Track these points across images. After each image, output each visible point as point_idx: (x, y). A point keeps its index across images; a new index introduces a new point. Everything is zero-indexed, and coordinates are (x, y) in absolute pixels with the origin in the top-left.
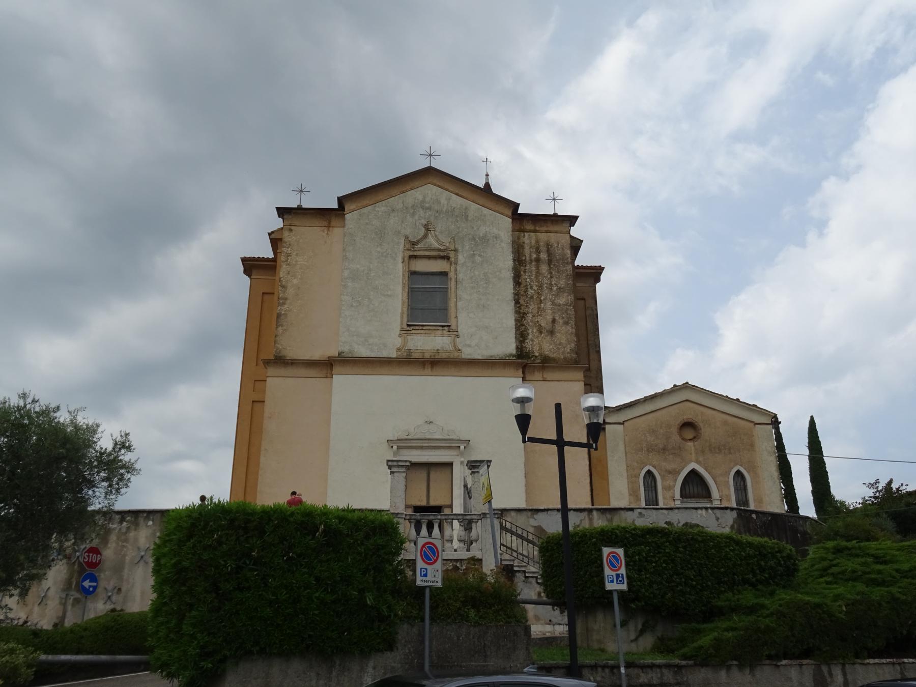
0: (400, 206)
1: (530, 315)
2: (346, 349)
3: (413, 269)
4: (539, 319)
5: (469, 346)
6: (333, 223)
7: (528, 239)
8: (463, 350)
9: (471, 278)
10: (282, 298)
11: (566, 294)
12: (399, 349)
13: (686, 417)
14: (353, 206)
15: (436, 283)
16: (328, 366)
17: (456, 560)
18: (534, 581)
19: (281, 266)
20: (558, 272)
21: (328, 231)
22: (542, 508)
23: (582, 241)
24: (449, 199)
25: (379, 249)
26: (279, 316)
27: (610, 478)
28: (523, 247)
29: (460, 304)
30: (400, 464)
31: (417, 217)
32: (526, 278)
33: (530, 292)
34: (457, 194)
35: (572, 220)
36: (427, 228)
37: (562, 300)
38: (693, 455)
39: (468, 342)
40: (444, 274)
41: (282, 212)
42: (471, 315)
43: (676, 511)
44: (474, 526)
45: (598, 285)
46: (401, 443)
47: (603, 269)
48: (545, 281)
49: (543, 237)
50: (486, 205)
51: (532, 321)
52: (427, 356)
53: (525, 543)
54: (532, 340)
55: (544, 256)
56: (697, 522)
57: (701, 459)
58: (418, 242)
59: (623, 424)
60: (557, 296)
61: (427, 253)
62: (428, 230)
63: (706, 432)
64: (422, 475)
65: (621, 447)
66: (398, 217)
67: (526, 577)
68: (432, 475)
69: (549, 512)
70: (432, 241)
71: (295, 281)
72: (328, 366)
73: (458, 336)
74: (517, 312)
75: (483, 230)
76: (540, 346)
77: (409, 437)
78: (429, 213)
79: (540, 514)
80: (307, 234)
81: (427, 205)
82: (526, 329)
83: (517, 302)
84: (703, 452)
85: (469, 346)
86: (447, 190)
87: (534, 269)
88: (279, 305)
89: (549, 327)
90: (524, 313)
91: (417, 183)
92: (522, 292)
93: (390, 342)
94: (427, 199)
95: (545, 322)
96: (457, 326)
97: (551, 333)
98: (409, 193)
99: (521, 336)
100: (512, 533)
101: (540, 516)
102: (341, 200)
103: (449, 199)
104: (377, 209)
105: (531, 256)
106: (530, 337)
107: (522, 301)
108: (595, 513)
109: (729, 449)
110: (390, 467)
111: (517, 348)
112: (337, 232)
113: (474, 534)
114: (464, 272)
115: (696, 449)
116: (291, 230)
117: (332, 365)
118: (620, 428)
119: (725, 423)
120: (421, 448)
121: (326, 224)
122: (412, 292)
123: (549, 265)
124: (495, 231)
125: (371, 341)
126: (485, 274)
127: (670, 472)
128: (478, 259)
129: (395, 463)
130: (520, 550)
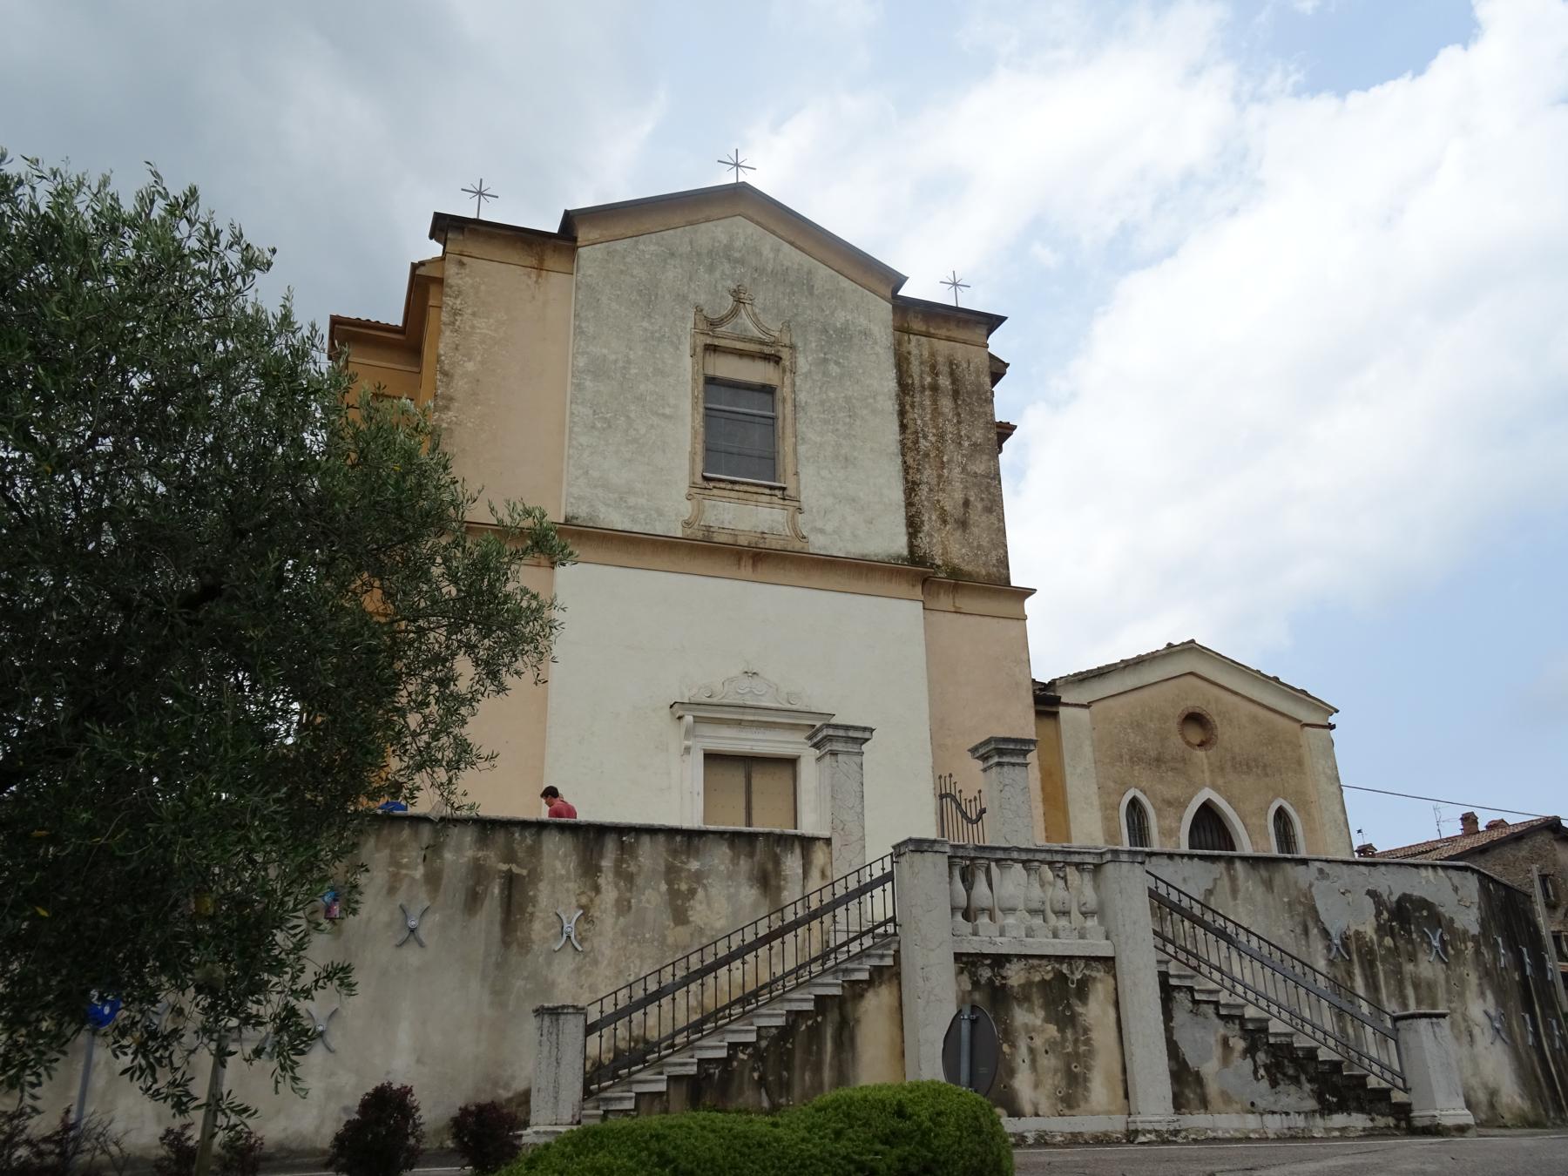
0: (686, 248)
1: (925, 488)
2: (582, 511)
3: (711, 372)
5: (822, 531)
6: (550, 262)
7: (917, 347)
8: (812, 538)
9: (822, 403)
11: (985, 457)
12: (687, 524)
13: (1192, 703)
14: (594, 234)
18: (1210, 1010)
19: (439, 332)
20: (972, 413)
21: (539, 276)
25: (645, 324)
29: (802, 449)
31: (717, 274)
33: (923, 444)
34: (792, 244)
35: (993, 322)
36: (738, 297)
38: (1207, 774)
39: (819, 524)
40: (768, 390)
41: (444, 226)
42: (824, 473)
43: (1383, 868)
47: (1014, 428)
49: (942, 347)
50: (798, 243)
51: (928, 499)
52: (743, 541)
55: (944, 382)
56: (1424, 895)
57: (1220, 782)
58: (721, 321)
59: (1087, 706)
60: (970, 457)
61: (739, 345)
62: (739, 301)
63: (1225, 732)
64: (736, 778)
65: (1088, 750)
67: (1195, 1002)
68: (755, 782)
75: (841, 317)
76: (945, 548)
77: (714, 700)
78: (740, 270)
79: (1154, 859)
80: (486, 280)
81: (737, 255)
84: (1222, 769)
85: (822, 531)
86: (774, 233)
87: (927, 403)
90: (914, 483)
93: (670, 506)
94: (738, 244)
96: (799, 492)
97: (963, 524)
98: (703, 226)
104: (641, 247)
106: (926, 528)
108: (1238, 865)
109: (1265, 766)
112: (556, 282)
114: (807, 391)
115: (1210, 764)
116: (462, 264)
118: (1084, 713)
119: (1255, 719)
121: (534, 262)
124: (863, 321)
125: (632, 501)
126: (848, 399)
127: (1169, 803)
128: (834, 369)
129: (841, 733)
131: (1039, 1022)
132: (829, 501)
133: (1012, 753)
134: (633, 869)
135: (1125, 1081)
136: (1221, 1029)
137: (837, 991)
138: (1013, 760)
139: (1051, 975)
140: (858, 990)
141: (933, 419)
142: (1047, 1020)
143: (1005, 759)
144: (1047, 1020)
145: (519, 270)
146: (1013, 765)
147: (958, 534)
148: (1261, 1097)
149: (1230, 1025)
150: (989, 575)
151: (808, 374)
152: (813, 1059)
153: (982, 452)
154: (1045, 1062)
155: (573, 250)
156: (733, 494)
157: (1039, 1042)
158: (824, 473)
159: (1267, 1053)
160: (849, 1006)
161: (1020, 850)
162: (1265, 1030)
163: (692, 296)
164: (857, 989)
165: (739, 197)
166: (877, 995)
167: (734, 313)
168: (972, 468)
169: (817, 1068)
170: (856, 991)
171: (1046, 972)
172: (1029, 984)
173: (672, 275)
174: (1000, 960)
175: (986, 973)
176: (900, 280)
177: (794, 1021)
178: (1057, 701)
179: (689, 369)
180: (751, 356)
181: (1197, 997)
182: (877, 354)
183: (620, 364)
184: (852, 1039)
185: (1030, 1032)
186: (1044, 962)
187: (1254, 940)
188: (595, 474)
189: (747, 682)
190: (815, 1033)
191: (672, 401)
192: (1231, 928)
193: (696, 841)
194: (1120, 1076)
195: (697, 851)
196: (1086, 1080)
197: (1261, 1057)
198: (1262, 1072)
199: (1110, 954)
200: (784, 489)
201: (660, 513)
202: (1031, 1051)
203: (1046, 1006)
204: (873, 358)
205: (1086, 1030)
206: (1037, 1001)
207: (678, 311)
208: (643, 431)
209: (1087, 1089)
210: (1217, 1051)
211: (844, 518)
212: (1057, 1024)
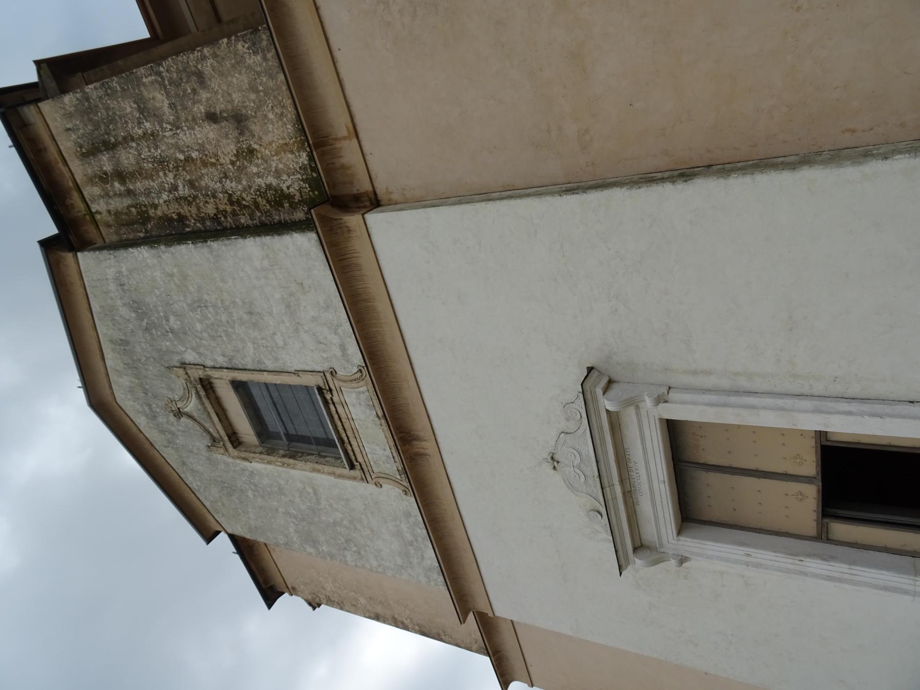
1: (228, 185)
4: (225, 160)
7: (103, 204)
15: (271, 389)
23: (38, 63)
28: (117, 214)
29: (270, 365)
33: (183, 191)
36: (179, 414)
37: (160, 100)
46: (633, 545)
51: (239, 181)
60: (157, 116)
89: (228, 127)
106: (272, 180)
158: (280, 343)
176: (46, 244)
180: (213, 421)
188: (399, 561)
211: (314, 319)
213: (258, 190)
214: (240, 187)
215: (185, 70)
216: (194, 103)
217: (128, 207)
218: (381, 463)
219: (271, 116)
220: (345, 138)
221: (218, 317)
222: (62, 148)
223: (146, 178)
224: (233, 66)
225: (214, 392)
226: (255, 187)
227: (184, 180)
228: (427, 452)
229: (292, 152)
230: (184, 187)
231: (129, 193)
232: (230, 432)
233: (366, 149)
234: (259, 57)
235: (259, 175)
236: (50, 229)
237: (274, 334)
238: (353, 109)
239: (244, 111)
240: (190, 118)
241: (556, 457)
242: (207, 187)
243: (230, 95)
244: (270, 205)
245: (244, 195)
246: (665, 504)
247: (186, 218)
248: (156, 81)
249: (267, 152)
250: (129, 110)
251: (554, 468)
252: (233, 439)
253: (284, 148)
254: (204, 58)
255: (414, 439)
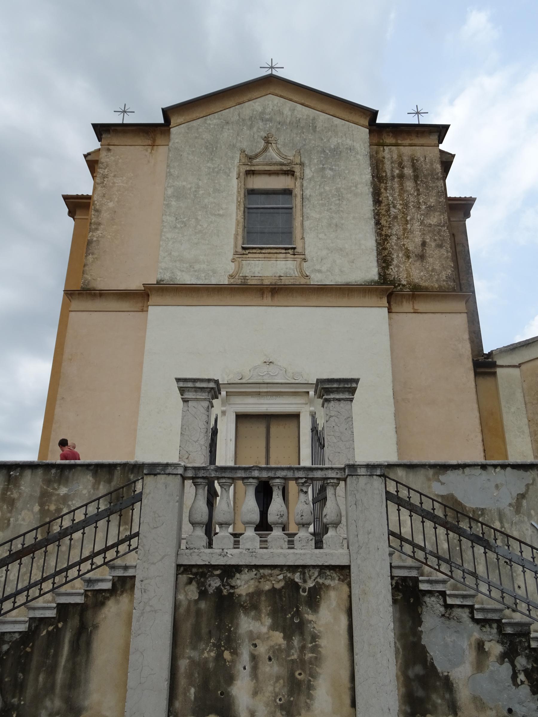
0: (236, 118)
1: (394, 238)
2: (167, 277)
3: (250, 186)
4: (406, 241)
5: (320, 271)
6: (159, 141)
7: (389, 154)
8: (312, 276)
10: (95, 224)
11: (437, 214)
12: (231, 276)
14: (180, 120)
15: (279, 202)
16: (143, 296)
17: (293, 568)
18: (465, 614)
20: (427, 188)
21: (152, 150)
22: (454, 462)
23: (454, 156)
24: (293, 110)
25: (209, 165)
26: (90, 243)
27: (507, 436)
28: (383, 162)
29: (307, 223)
30: (198, 385)
31: (255, 129)
32: (388, 196)
33: (393, 211)
34: (302, 104)
35: (440, 131)
36: (267, 141)
37: (433, 220)
39: (318, 267)
40: (288, 192)
41: (101, 130)
44: (330, 492)
45: (468, 221)
48: (412, 199)
49: (406, 151)
50: (337, 115)
51: (396, 244)
52: (266, 282)
53: (429, 524)
54: (398, 266)
55: (408, 171)
58: (256, 156)
60: (426, 215)
61: (267, 168)
64: (260, 429)
65: (519, 395)
66: (234, 131)
69: (467, 470)
70: (272, 154)
71: (111, 205)
72: (143, 296)
73: (305, 260)
74: (379, 234)
75: (334, 142)
77: (243, 381)
80: (130, 152)
81: (268, 117)
82: (390, 254)
83: (378, 223)
85: (320, 271)
86: (291, 100)
87: (396, 185)
88: (91, 230)
89: (418, 250)
90: (386, 235)
91: (256, 94)
92: (383, 212)
93: (221, 267)
94: (268, 110)
95: (413, 243)
97: (422, 257)
98: (246, 104)
99: (384, 261)
100: (412, 509)
101: (451, 476)
102: (167, 112)
103: (293, 110)
104: (208, 122)
105: (392, 171)
106: (395, 262)
107: (383, 222)
110: (182, 390)
111: (379, 274)
112: (162, 151)
113: (330, 510)
114: (311, 187)
116: (109, 150)
117: (148, 295)
118: (516, 372)
120: (259, 394)
121: (150, 142)
122: (249, 212)
123: (416, 182)
124: (349, 142)
125: (197, 267)
128: (329, 173)
129: (190, 385)
130: (419, 540)
131: (264, 630)
132: (325, 252)
133: (338, 390)
134: (15, 495)
135: (353, 689)
136: (476, 633)
137: (80, 600)
138: (337, 396)
139: (282, 584)
140: (100, 598)
141: (400, 195)
142: (274, 627)
143: (332, 396)
144: (274, 627)
145: (141, 148)
146: (339, 400)
147: (418, 264)
148: (521, 703)
149: (487, 629)
150: (440, 287)
151: (310, 179)
152: (49, 662)
153: (435, 211)
154: (268, 669)
155: (169, 132)
156: (261, 255)
157: (262, 649)
158: (321, 236)
159: (528, 657)
160: (89, 614)
161: (282, 469)
162: (527, 634)
163: (238, 145)
164: (100, 598)
165: (270, 83)
166: (118, 602)
167: (265, 149)
168: (428, 221)
169: (52, 671)
170: (97, 599)
171: (278, 581)
172: (258, 593)
173: (226, 135)
174: (230, 571)
175: (214, 583)
176: (374, 114)
177: (37, 627)
178: (494, 365)
179: (236, 186)
180: (276, 173)
181: (449, 601)
182: (358, 160)
183: (193, 189)
184: (89, 644)
185: (254, 639)
186: (276, 572)
187: (515, 545)
188: (175, 254)
189: (265, 368)
190: (55, 638)
191: (224, 206)
192: (490, 536)
193: (66, 473)
194: (348, 685)
195: (67, 480)
196: (310, 687)
197: (521, 662)
198: (522, 677)
199: (344, 562)
200: (294, 248)
201: (214, 272)
202: (254, 658)
203: (273, 614)
204: (356, 162)
205: (314, 637)
206: (265, 608)
207: (230, 154)
208: (205, 225)
209: (310, 697)
210: (471, 656)
211: (334, 261)
212: (284, 631)
213: (391, 253)
214: (393, 244)
215: (444, 240)
216: (430, 237)
217: (385, 171)
218: (250, 267)
219: (422, 274)
220: (413, 307)
221: (333, 204)
222: (417, 148)
223: (399, 192)
224: (442, 264)
225: (282, 174)
226: (393, 252)
227: (398, 214)
228: (265, 299)
229: (407, 278)
230: (395, 212)
231: (393, 177)
232: (255, 172)
233: (408, 314)
234: (445, 278)
235: (398, 256)
236: (380, 120)
237: (325, 235)
238: (424, 314)
239: (425, 261)
240: (425, 232)
241: (271, 364)
242: (394, 226)
243: (432, 257)
244: (384, 256)
245: (389, 244)
246: (254, 409)
247: (380, 206)
248: (441, 222)
249: (407, 265)
250: (431, 200)
251: (265, 362)
252: (251, 172)
253: (409, 275)
254: (447, 252)
255: (272, 294)
